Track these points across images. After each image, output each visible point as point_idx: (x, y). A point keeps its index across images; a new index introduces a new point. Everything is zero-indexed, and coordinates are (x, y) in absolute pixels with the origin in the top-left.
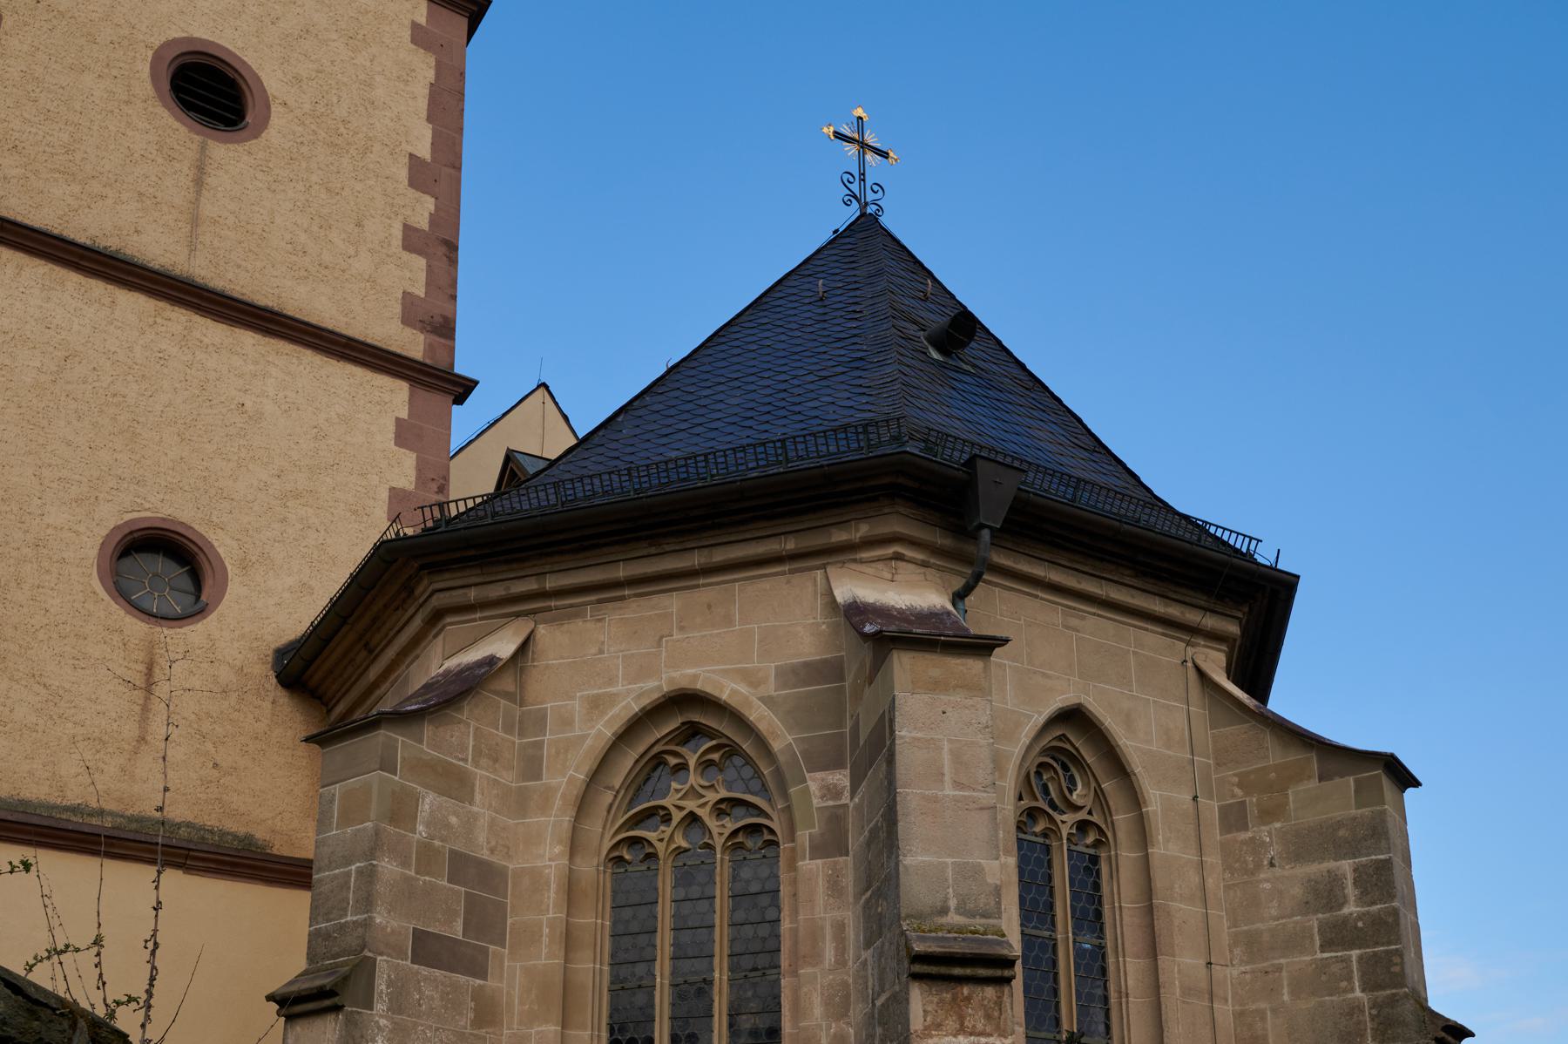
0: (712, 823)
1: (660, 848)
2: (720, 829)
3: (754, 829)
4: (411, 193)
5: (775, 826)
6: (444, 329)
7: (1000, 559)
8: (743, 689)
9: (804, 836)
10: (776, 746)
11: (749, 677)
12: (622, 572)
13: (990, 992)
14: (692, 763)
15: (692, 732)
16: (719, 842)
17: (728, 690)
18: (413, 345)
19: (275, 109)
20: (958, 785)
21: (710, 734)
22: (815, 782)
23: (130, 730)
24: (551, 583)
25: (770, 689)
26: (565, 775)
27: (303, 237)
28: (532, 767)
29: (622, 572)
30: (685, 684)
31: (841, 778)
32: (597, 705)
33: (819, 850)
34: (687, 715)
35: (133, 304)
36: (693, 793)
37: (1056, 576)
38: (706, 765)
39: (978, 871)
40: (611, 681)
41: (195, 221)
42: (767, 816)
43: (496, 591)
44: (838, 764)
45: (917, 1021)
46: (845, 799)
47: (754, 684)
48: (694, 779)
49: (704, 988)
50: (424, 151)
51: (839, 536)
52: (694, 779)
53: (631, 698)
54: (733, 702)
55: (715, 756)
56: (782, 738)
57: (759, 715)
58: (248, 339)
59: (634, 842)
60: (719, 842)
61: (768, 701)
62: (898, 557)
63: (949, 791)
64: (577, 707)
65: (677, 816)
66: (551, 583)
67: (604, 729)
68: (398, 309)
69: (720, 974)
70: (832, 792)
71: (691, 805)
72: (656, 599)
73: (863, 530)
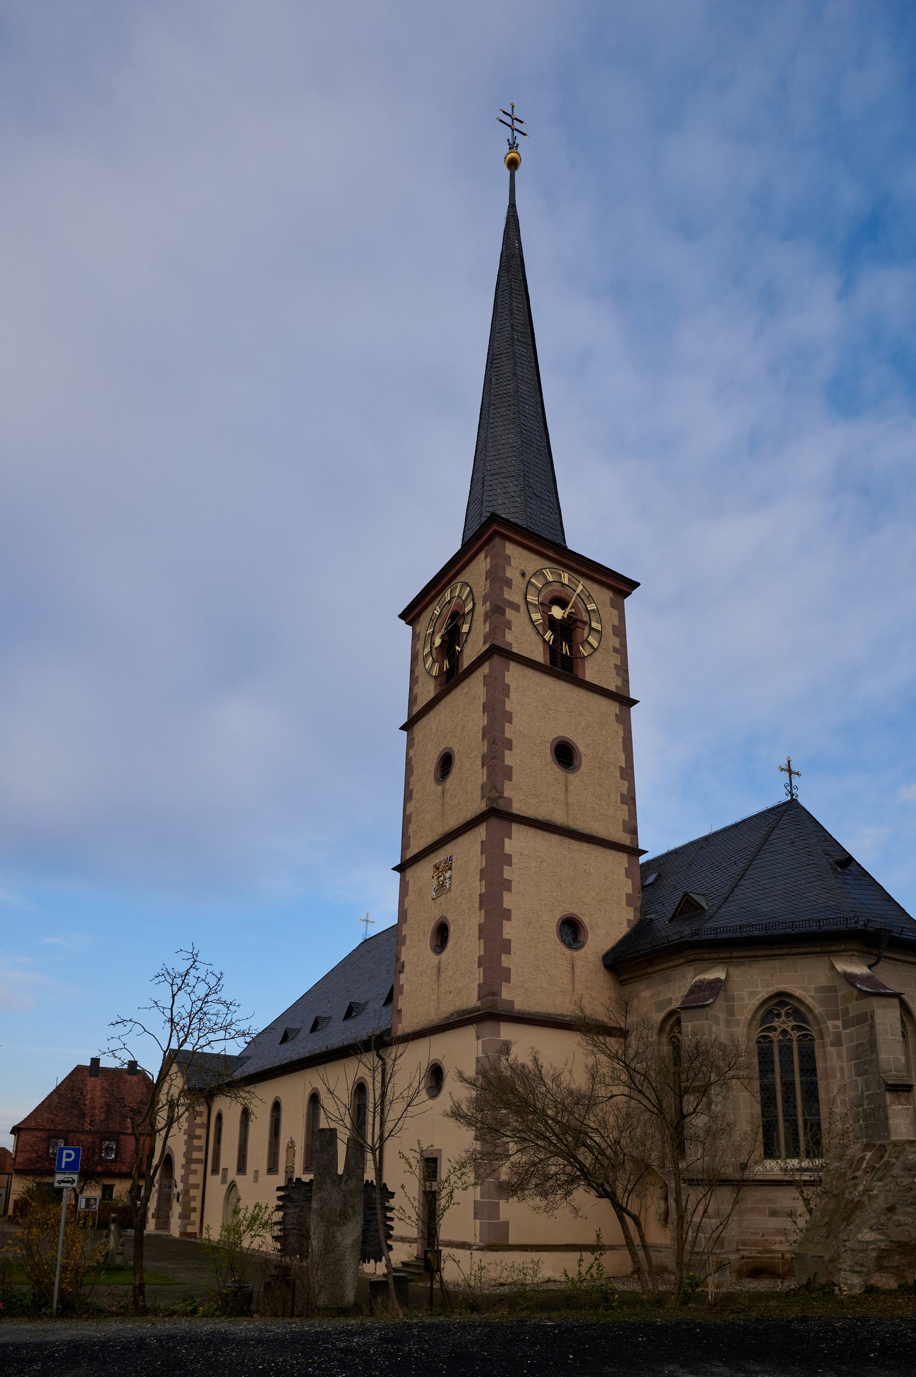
0: (792, 1033)
1: (775, 1040)
2: (795, 1035)
3: (805, 1035)
4: (622, 781)
5: (813, 1034)
6: (633, 831)
7: (885, 954)
8: (803, 993)
9: (828, 1040)
10: (816, 1012)
11: (803, 988)
12: (759, 953)
13: (906, 1094)
14: (783, 1012)
15: (782, 1004)
16: (795, 1039)
17: (798, 993)
18: (625, 839)
19: (583, 757)
20: (892, 1035)
21: (787, 1004)
22: (830, 1024)
23: (570, 988)
24: (734, 954)
25: (813, 993)
26: (744, 1016)
27: (595, 805)
28: (731, 1012)
29: (759, 953)
30: (783, 990)
31: (839, 1023)
32: (752, 994)
33: (833, 1044)
34: (781, 999)
35: (555, 838)
36: (784, 1022)
37: (893, 956)
38: (787, 1015)
39: (899, 1059)
40: (757, 987)
41: (567, 805)
42: (807, 1030)
43: (715, 956)
44: (838, 1019)
45: (888, 1102)
46: (841, 1029)
47: (807, 991)
48: (783, 1018)
49: (792, 1083)
50: (623, 765)
51: (834, 948)
52: (783, 1018)
53: (764, 992)
54: (800, 997)
55: (790, 1011)
56: (818, 1010)
57: (809, 1001)
58: (585, 846)
59: (764, 1037)
60: (795, 1039)
61: (812, 997)
62: (853, 955)
63: (890, 1037)
64: (745, 994)
65: (779, 1030)
66: (734, 954)
67: (756, 1002)
68: (621, 827)
69: (797, 1079)
70: (835, 1027)
71: (784, 1026)
72: (770, 962)
73: (843, 947)
